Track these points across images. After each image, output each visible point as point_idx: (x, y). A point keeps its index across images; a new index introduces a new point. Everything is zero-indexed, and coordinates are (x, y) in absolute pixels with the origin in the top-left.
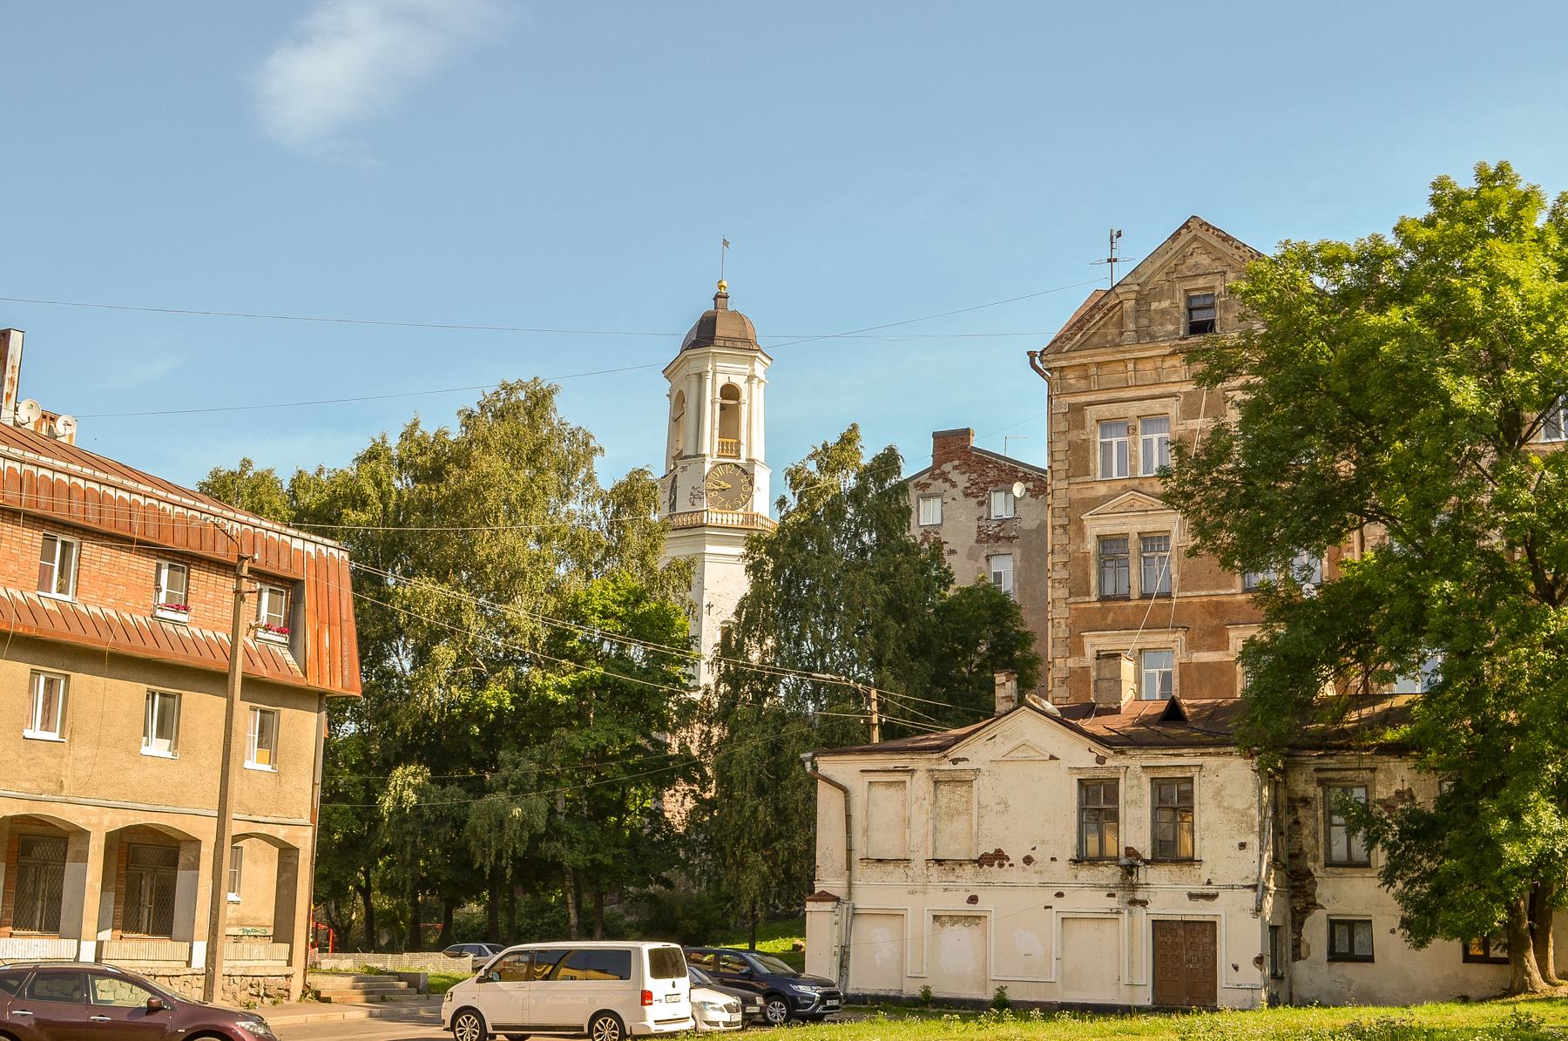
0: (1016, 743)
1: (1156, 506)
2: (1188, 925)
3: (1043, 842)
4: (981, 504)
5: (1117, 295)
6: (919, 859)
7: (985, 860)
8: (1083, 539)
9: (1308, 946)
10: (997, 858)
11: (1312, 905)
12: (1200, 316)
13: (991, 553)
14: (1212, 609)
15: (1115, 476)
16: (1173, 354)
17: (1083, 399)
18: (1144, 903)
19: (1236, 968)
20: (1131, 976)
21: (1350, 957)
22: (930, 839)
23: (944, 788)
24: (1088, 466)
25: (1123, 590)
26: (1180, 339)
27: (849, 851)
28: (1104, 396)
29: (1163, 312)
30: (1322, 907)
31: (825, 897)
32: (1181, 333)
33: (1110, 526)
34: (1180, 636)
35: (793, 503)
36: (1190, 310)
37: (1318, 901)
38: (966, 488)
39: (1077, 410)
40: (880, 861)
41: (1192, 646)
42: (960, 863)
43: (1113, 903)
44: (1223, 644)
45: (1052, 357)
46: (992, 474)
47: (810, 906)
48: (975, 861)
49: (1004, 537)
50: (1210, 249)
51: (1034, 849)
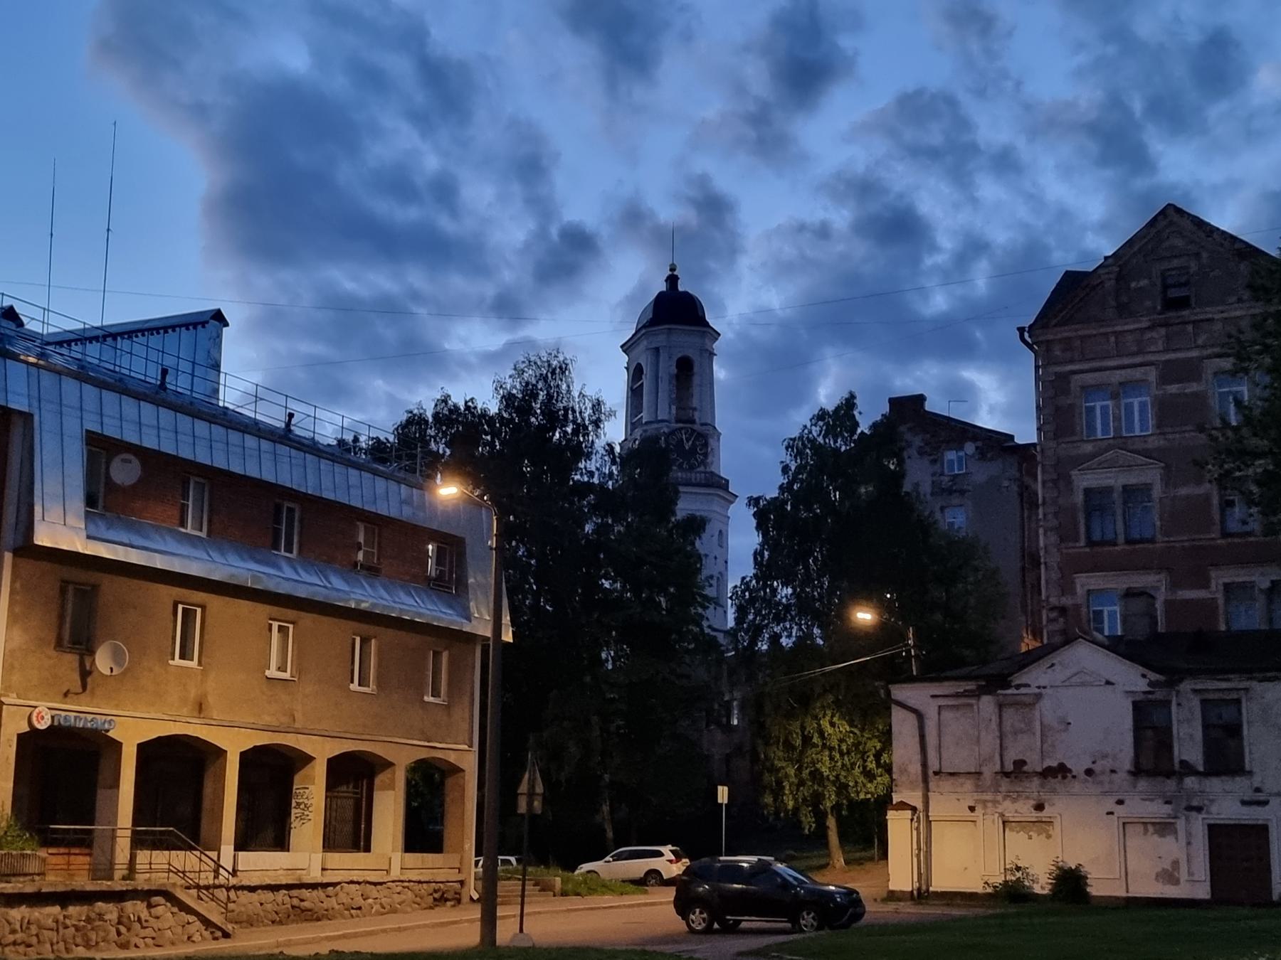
0: (1074, 670)
1: (1139, 462)
4: (934, 462)
5: (1100, 277)
10: (1061, 771)
12: (1173, 293)
13: (945, 504)
15: (1100, 436)
19: (966, 869)
25: (1109, 536)
26: (1160, 314)
28: (1086, 366)
31: (903, 806)
32: (1159, 308)
34: (1163, 576)
38: (921, 447)
39: (1064, 378)
41: (1174, 585)
49: (955, 491)
51: (1094, 763)
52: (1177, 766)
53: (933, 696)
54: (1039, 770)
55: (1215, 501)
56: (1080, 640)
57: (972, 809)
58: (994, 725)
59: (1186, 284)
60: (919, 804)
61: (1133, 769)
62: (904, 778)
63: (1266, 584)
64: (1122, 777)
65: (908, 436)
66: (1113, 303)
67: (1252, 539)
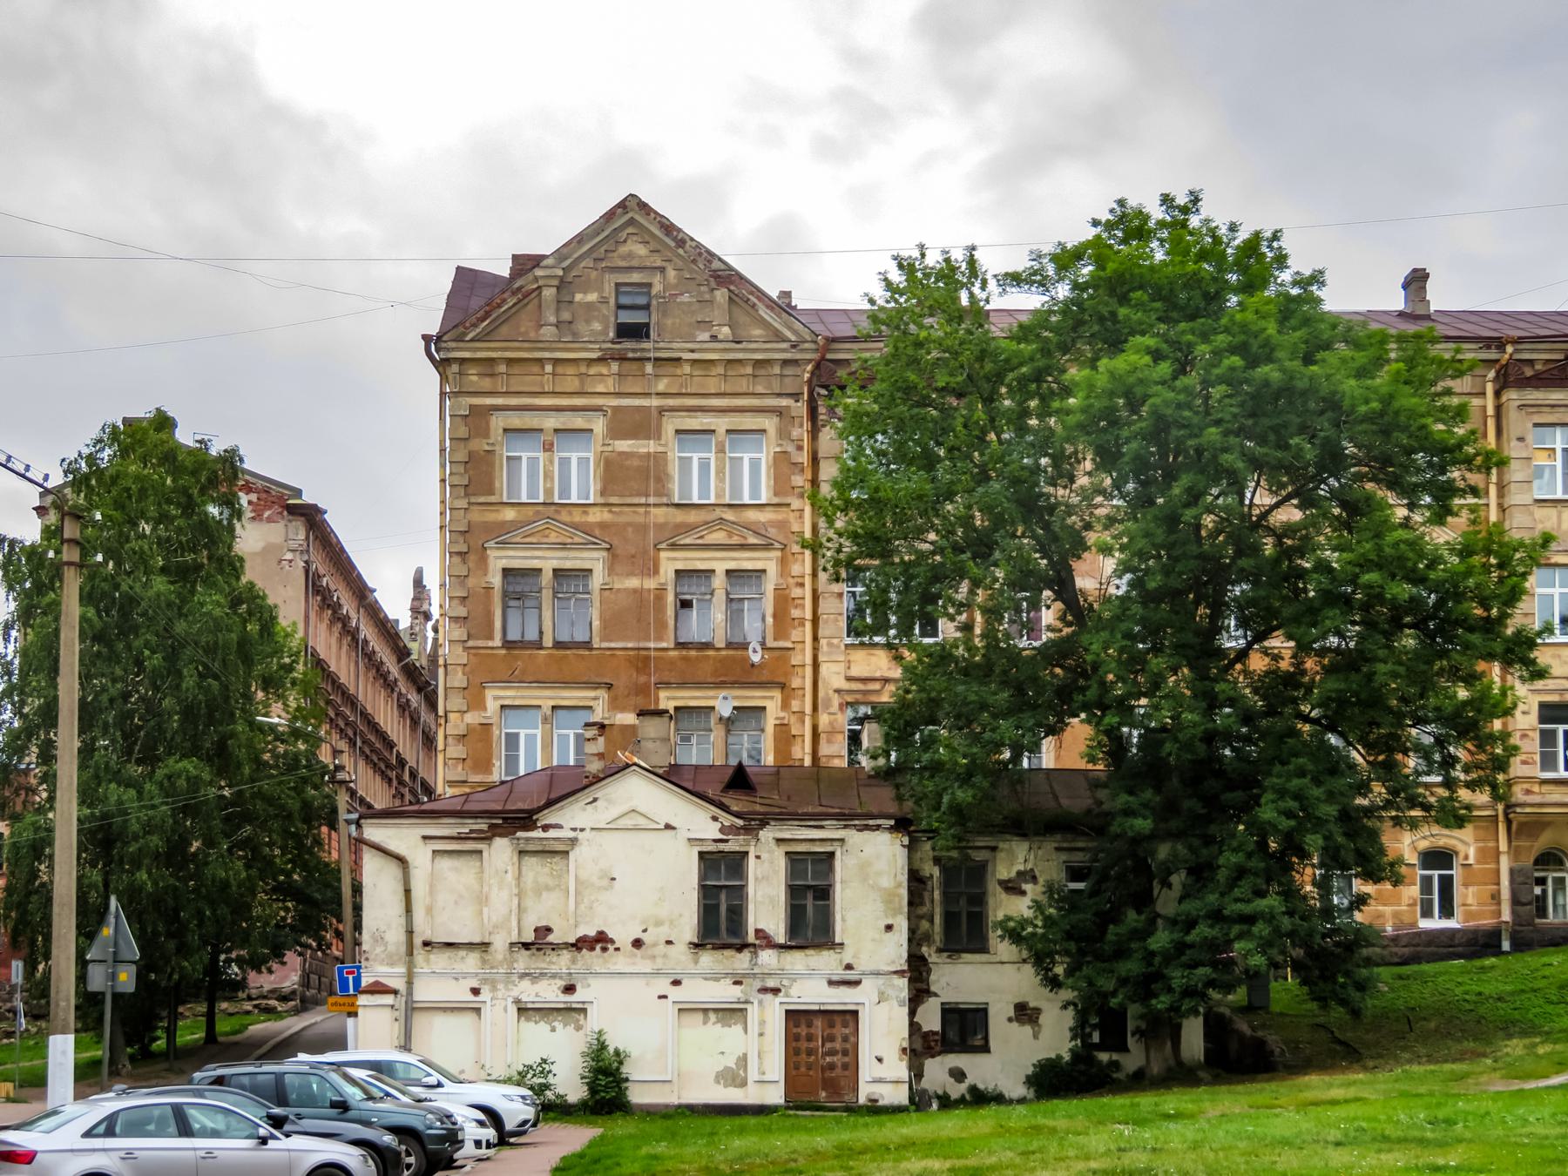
1: (577, 540)
2: (828, 1015)
6: (500, 944)
10: (601, 941)
12: (628, 317)
14: (640, 665)
15: (524, 499)
17: (489, 401)
23: (530, 861)
25: (532, 635)
27: (410, 932)
30: (936, 995)
31: (378, 989)
33: (518, 559)
34: (602, 694)
37: (933, 988)
45: (453, 345)
48: (573, 945)
50: (647, 238)
51: (645, 931)
52: (751, 938)
53: (425, 838)
54: (572, 940)
55: (670, 598)
56: (634, 768)
57: (476, 991)
58: (510, 877)
60: (398, 984)
61: (696, 941)
62: (379, 950)
63: (725, 710)
64: (680, 952)
66: (552, 319)
67: (711, 653)
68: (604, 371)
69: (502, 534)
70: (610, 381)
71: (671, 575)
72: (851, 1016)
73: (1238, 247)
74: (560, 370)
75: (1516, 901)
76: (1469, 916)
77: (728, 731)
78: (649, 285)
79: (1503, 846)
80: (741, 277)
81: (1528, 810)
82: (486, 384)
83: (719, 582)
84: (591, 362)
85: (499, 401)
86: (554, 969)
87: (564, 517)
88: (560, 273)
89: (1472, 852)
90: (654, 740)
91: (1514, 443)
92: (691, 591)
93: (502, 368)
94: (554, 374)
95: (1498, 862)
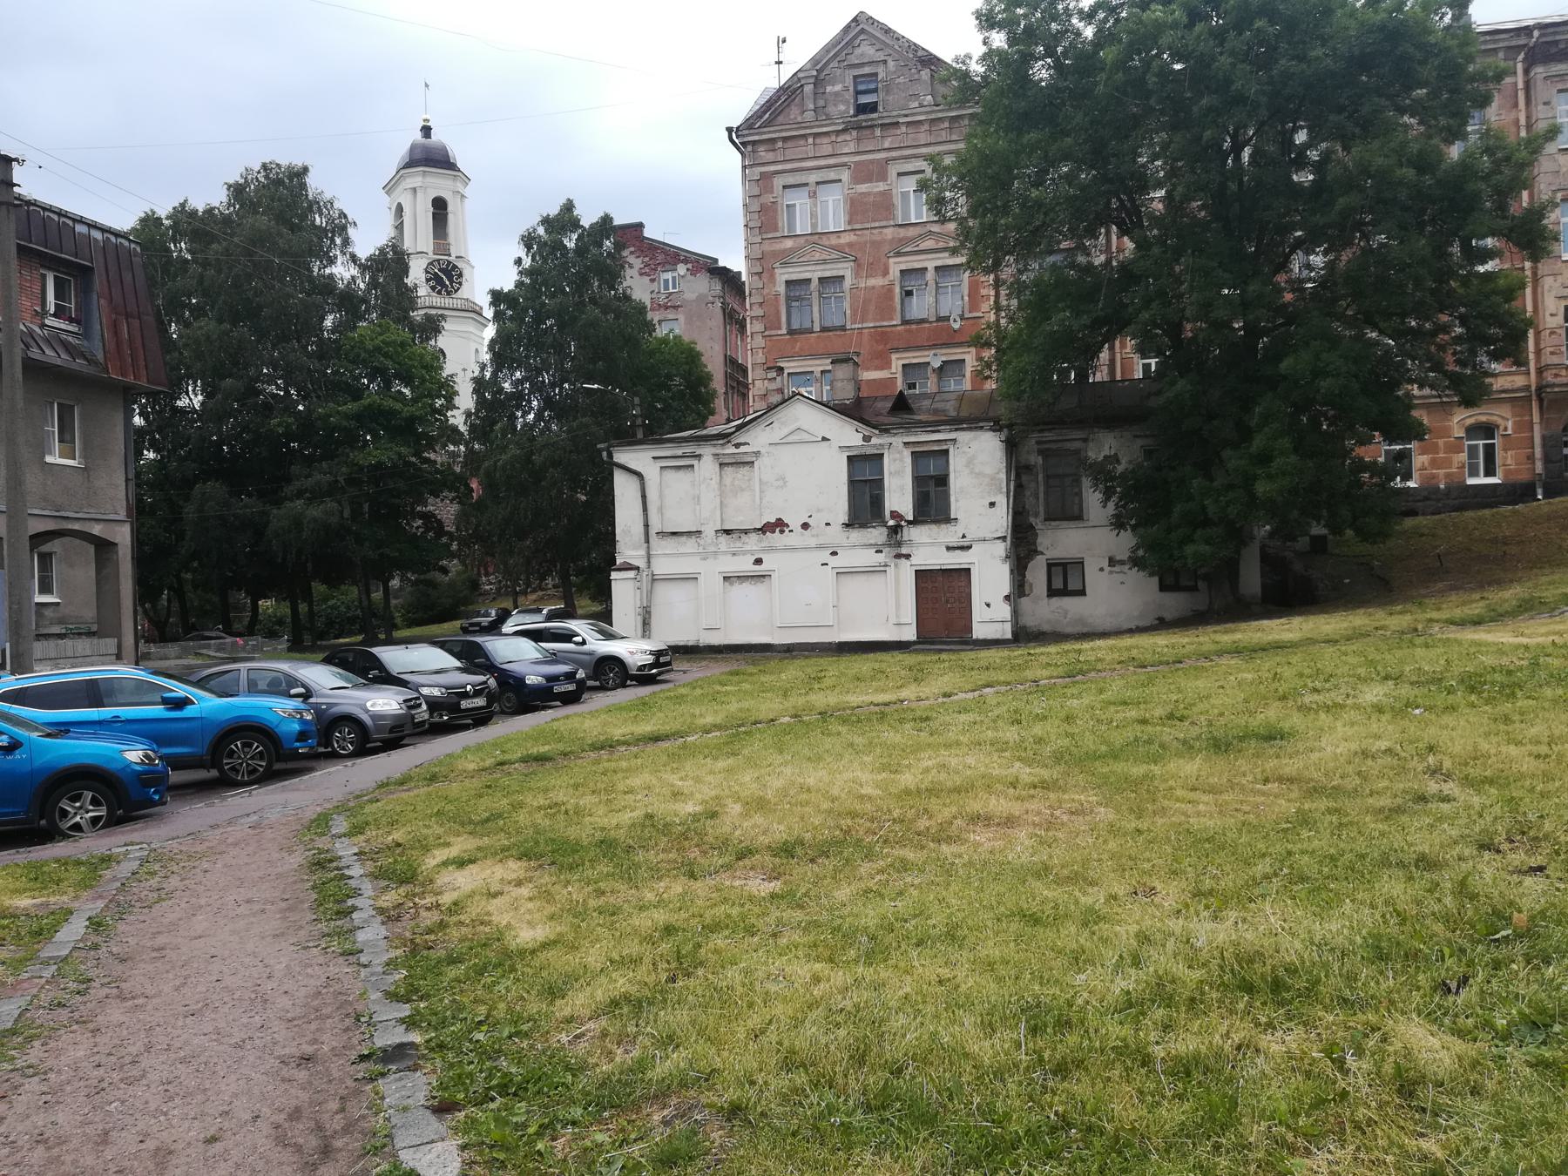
1: (834, 256)
3: (819, 510)
4: (652, 281)
6: (709, 531)
7: (767, 528)
8: (774, 283)
9: (1031, 585)
10: (779, 525)
11: (1034, 552)
12: (864, 99)
16: (844, 131)
18: (908, 556)
20: (897, 616)
21: (1064, 592)
22: (718, 513)
23: (728, 470)
24: (776, 224)
25: (807, 325)
27: (646, 526)
28: (789, 166)
29: (836, 94)
30: (1042, 553)
31: (628, 567)
35: (527, 262)
36: (858, 93)
40: (674, 534)
42: (746, 532)
43: (881, 558)
44: (887, 365)
45: (747, 132)
46: (660, 257)
47: (614, 575)
48: (759, 530)
55: (897, 290)
59: (875, 91)
60: (641, 563)
63: (937, 364)
64: (836, 528)
65: (631, 259)
67: (927, 325)
68: (848, 138)
69: (785, 258)
70: (852, 144)
71: (898, 274)
72: (963, 575)
73: (1438, 147)
74: (818, 141)
75: (1547, 460)
76: (1507, 473)
77: (940, 379)
78: (876, 75)
79: (1536, 418)
80: (939, 59)
81: (1556, 390)
82: (770, 156)
83: (930, 275)
84: (838, 133)
85: (779, 167)
86: (748, 548)
87: (825, 241)
88: (815, 73)
89: (1510, 424)
90: (842, 380)
91: (1540, 107)
92: (912, 284)
93: (780, 144)
94: (814, 145)
95: (1532, 431)
